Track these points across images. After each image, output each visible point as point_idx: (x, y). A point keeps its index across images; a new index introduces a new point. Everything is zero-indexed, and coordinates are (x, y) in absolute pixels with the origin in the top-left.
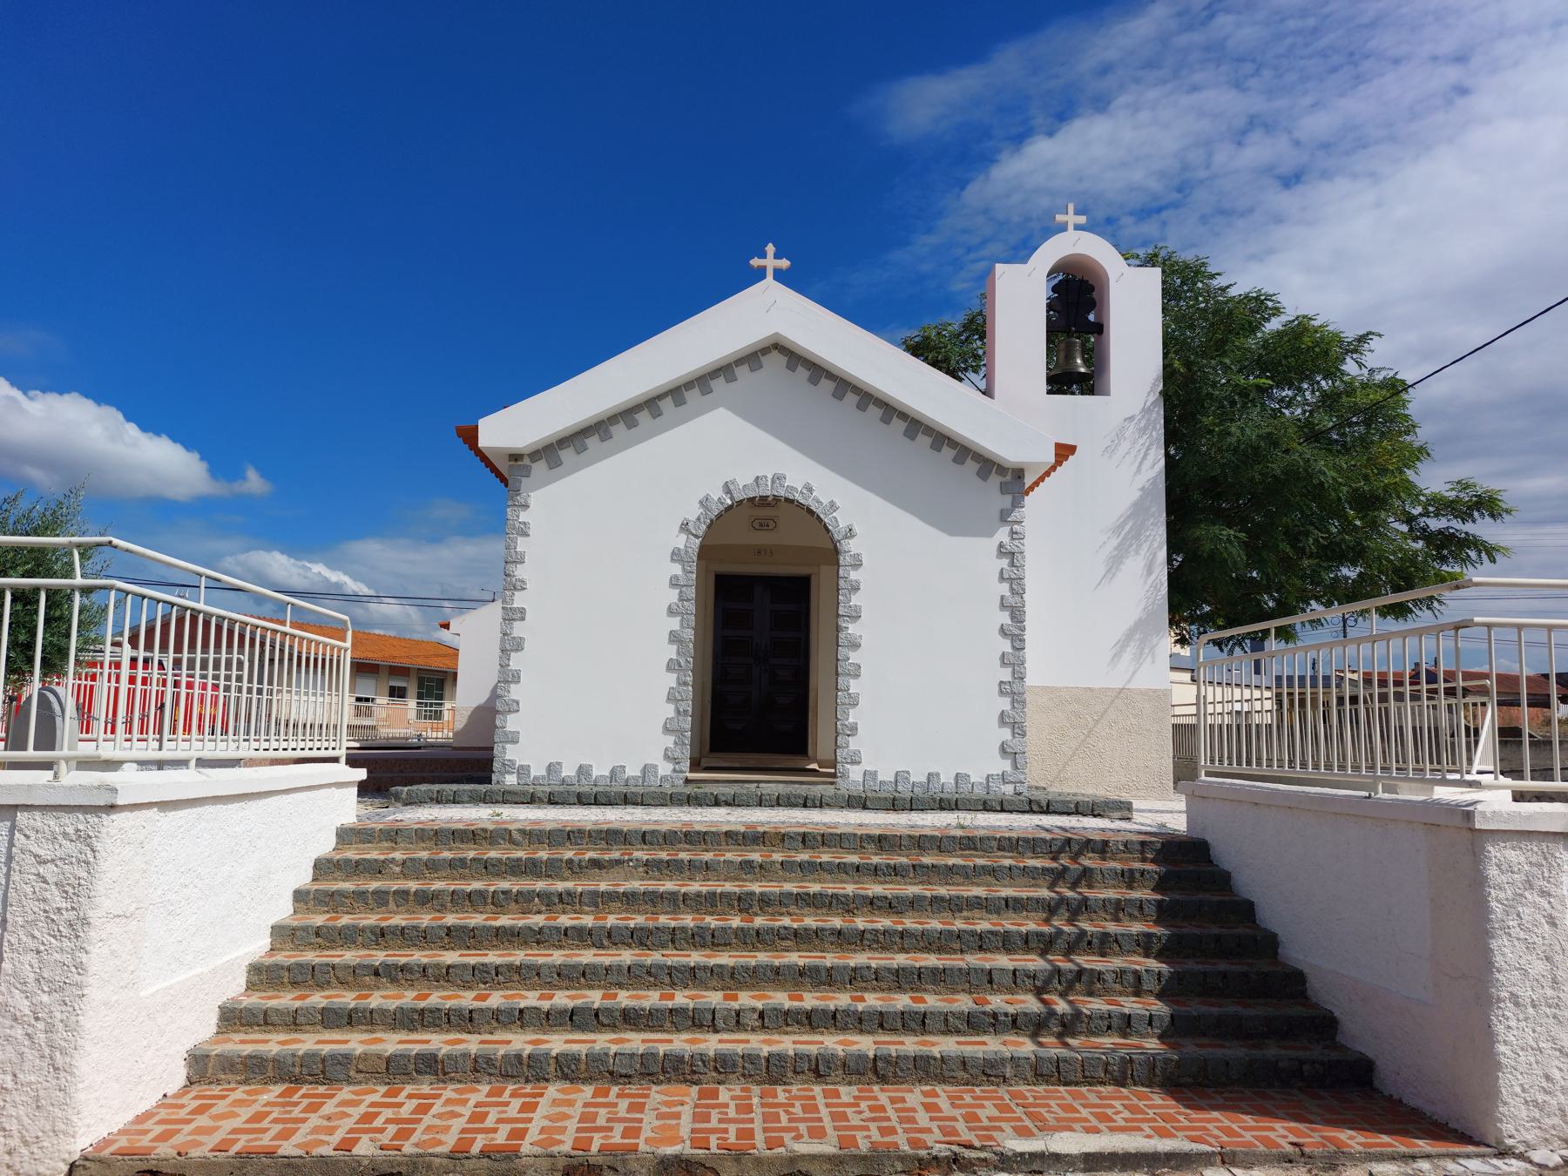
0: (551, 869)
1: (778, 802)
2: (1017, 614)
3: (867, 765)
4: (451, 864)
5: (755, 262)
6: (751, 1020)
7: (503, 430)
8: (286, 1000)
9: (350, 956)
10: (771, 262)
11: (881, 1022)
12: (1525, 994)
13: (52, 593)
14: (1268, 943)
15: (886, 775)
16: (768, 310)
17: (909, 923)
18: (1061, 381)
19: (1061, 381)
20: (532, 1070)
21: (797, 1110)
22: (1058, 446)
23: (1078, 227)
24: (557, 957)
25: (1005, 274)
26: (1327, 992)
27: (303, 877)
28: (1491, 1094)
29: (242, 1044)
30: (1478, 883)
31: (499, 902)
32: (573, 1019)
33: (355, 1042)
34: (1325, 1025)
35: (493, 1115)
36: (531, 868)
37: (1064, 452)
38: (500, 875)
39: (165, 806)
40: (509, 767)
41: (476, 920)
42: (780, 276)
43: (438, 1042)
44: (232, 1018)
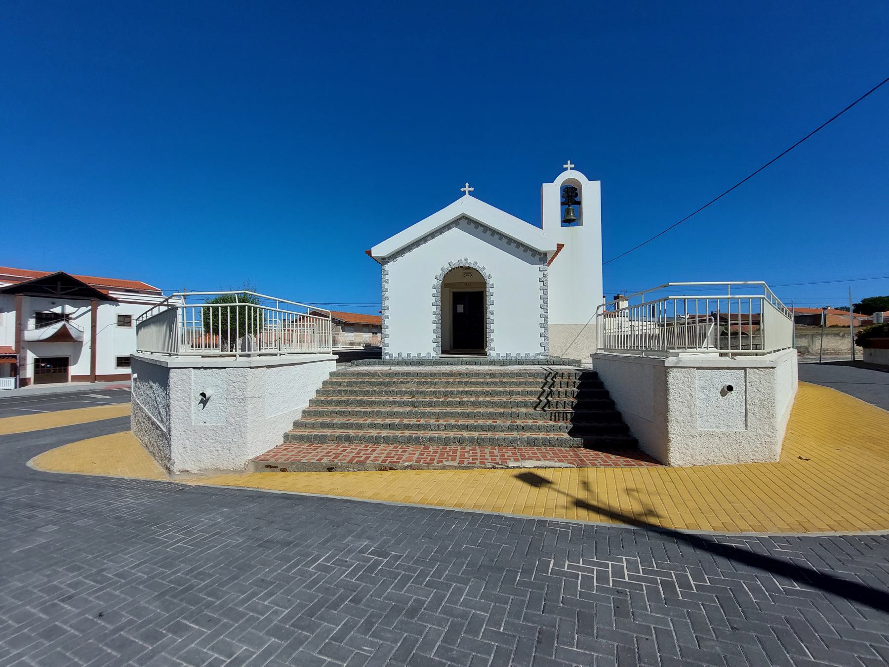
0: (389, 384)
1: (468, 363)
2: (545, 300)
3: (497, 351)
4: (360, 383)
5: (462, 189)
6: (443, 428)
7: (378, 251)
8: (312, 420)
9: (330, 408)
10: (467, 189)
11: (482, 428)
12: (680, 419)
13: (231, 307)
14: (612, 404)
15: (503, 354)
16: (468, 205)
17: (496, 399)
18: (567, 221)
19: (567, 221)
20: (376, 441)
21: (451, 453)
22: (558, 245)
23: (571, 169)
24: (388, 409)
25: (546, 187)
26: (628, 418)
27: (320, 386)
28: (667, 450)
29: (299, 432)
30: (666, 383)
31: (373, 393)
32: (391, 427)
33: (328, 432)
34: (625, 429)
35: (363, 452)
36: (384, 384)
37: (560, 247)
38: (375, 386)
39: (268, 367)
40: (387, 354)
41: (366, 398)
42: (470, 193)
43: (351, 432)
44: (296, 425)
